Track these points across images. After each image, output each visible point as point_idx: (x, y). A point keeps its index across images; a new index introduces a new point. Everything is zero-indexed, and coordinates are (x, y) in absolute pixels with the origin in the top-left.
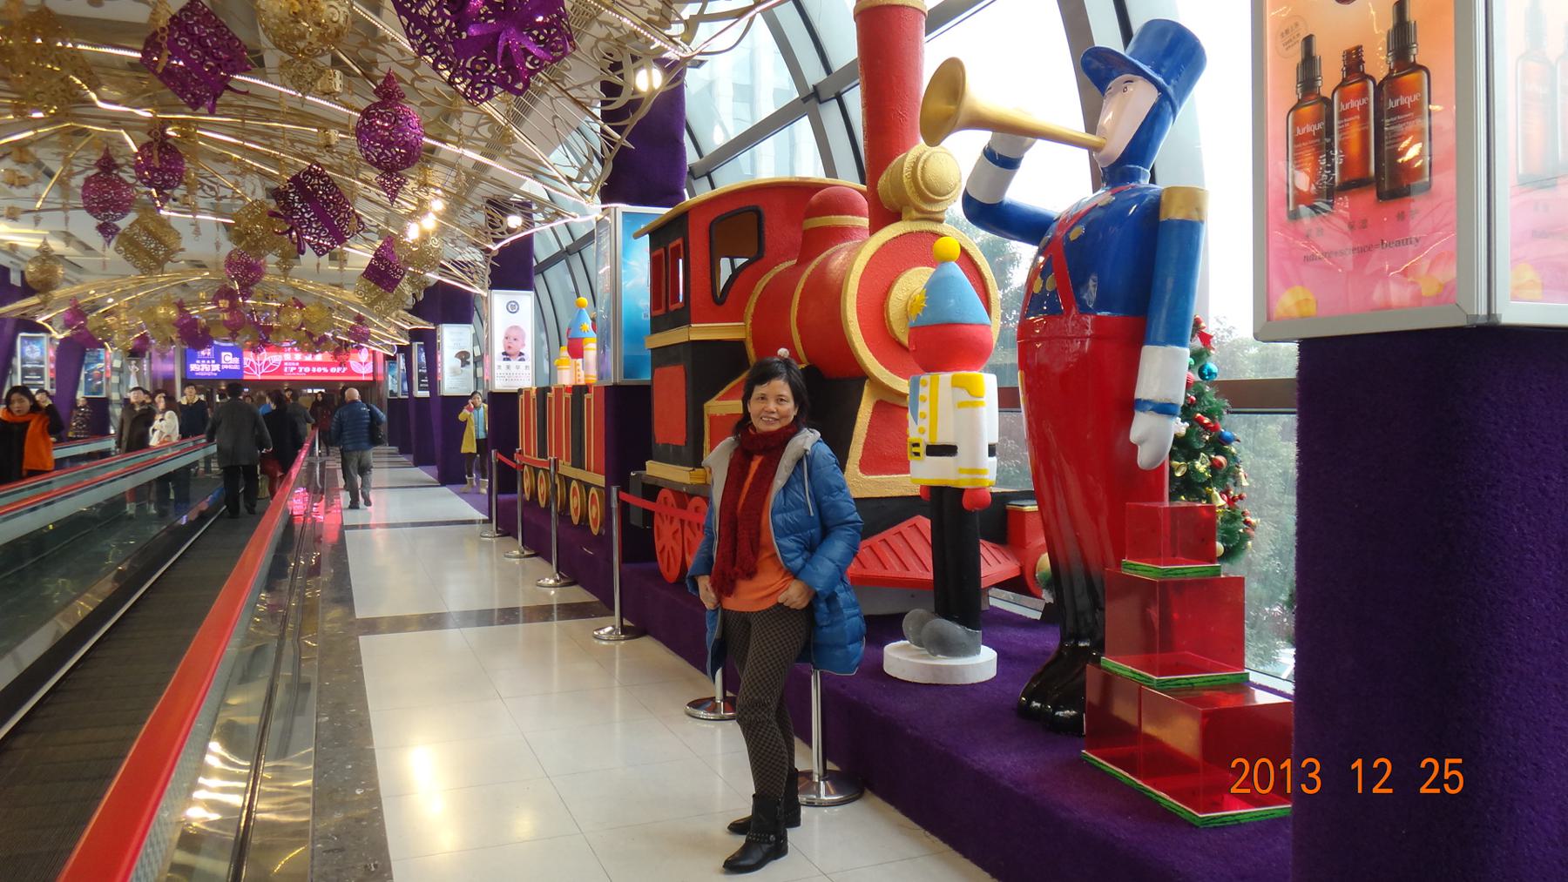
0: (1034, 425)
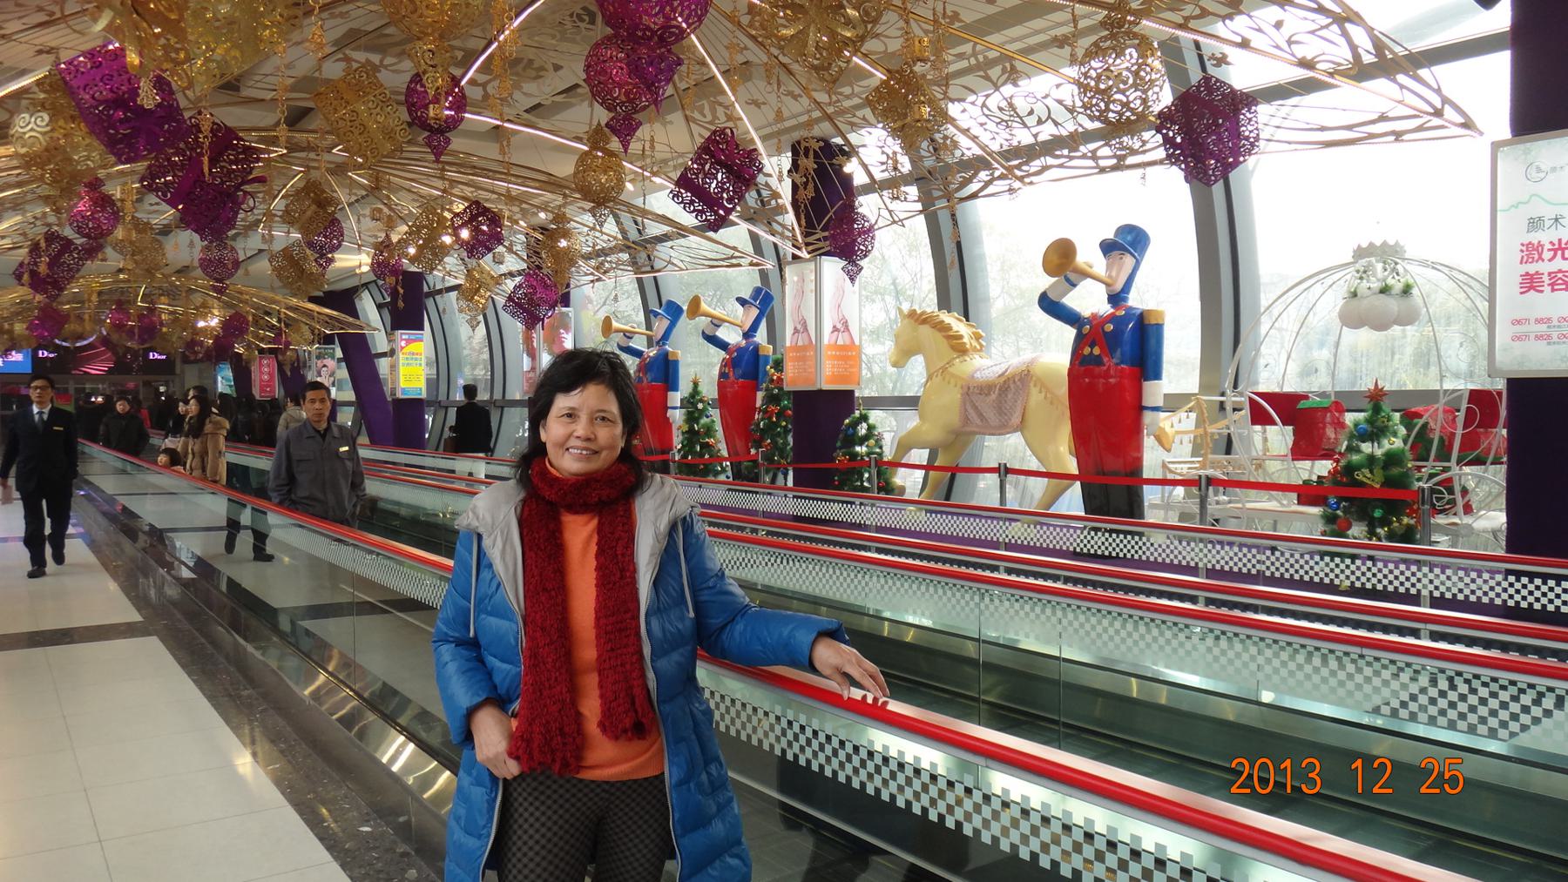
0: (730, 421)
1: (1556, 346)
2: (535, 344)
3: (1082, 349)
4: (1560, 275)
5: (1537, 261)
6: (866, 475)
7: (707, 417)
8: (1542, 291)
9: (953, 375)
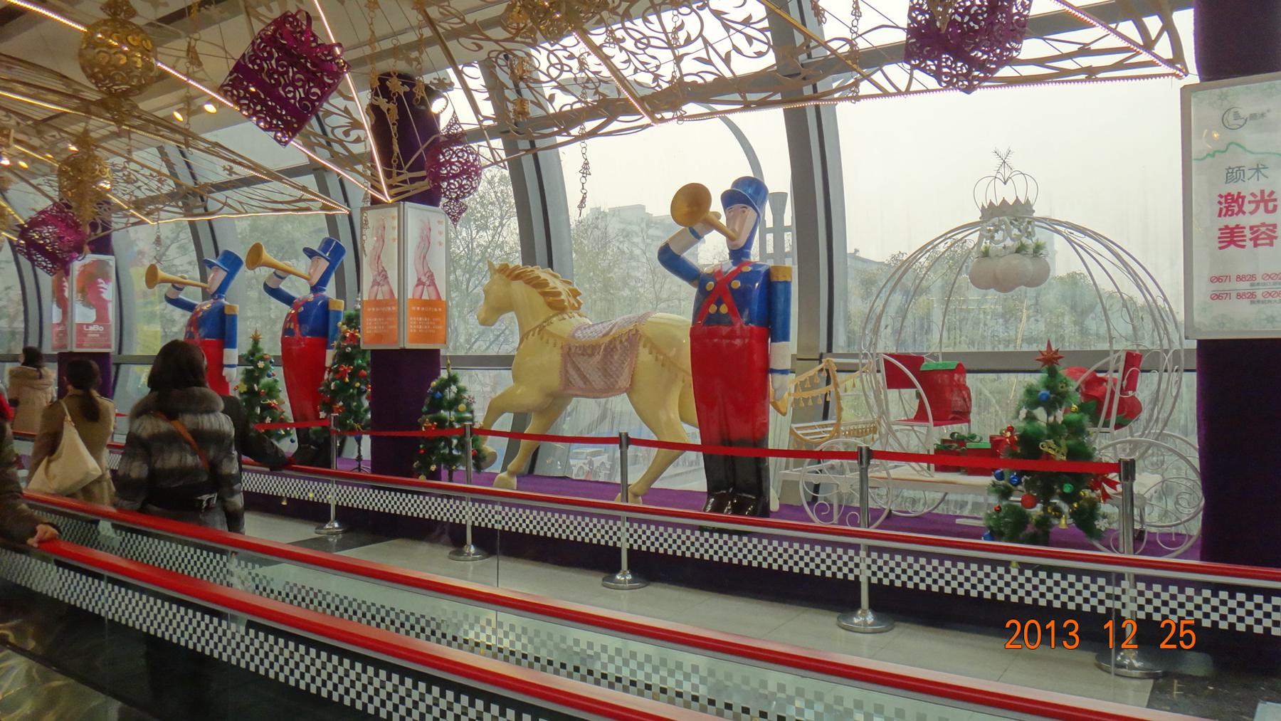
1: (1262, 306)
2: (66, 294)
3: (708, 306)
4: (1263, 229)
5: (1237, 214)
6: (455, 442)
7: (269, 376)
8: (1243, 247)
9: (552, 335)
